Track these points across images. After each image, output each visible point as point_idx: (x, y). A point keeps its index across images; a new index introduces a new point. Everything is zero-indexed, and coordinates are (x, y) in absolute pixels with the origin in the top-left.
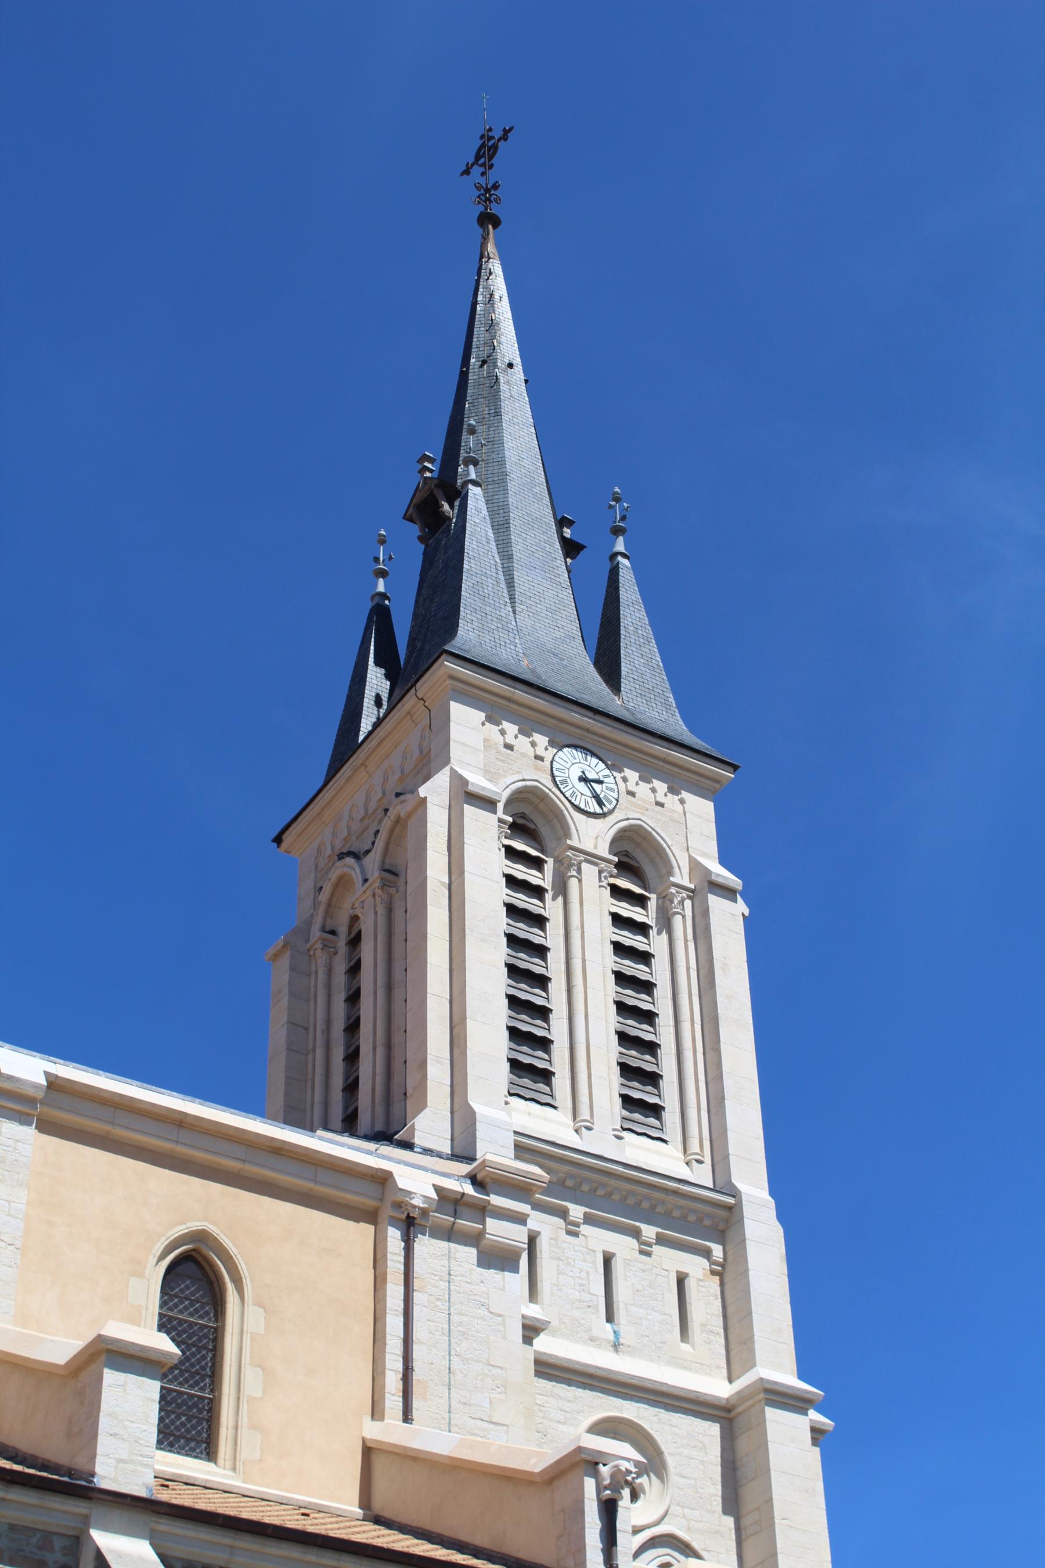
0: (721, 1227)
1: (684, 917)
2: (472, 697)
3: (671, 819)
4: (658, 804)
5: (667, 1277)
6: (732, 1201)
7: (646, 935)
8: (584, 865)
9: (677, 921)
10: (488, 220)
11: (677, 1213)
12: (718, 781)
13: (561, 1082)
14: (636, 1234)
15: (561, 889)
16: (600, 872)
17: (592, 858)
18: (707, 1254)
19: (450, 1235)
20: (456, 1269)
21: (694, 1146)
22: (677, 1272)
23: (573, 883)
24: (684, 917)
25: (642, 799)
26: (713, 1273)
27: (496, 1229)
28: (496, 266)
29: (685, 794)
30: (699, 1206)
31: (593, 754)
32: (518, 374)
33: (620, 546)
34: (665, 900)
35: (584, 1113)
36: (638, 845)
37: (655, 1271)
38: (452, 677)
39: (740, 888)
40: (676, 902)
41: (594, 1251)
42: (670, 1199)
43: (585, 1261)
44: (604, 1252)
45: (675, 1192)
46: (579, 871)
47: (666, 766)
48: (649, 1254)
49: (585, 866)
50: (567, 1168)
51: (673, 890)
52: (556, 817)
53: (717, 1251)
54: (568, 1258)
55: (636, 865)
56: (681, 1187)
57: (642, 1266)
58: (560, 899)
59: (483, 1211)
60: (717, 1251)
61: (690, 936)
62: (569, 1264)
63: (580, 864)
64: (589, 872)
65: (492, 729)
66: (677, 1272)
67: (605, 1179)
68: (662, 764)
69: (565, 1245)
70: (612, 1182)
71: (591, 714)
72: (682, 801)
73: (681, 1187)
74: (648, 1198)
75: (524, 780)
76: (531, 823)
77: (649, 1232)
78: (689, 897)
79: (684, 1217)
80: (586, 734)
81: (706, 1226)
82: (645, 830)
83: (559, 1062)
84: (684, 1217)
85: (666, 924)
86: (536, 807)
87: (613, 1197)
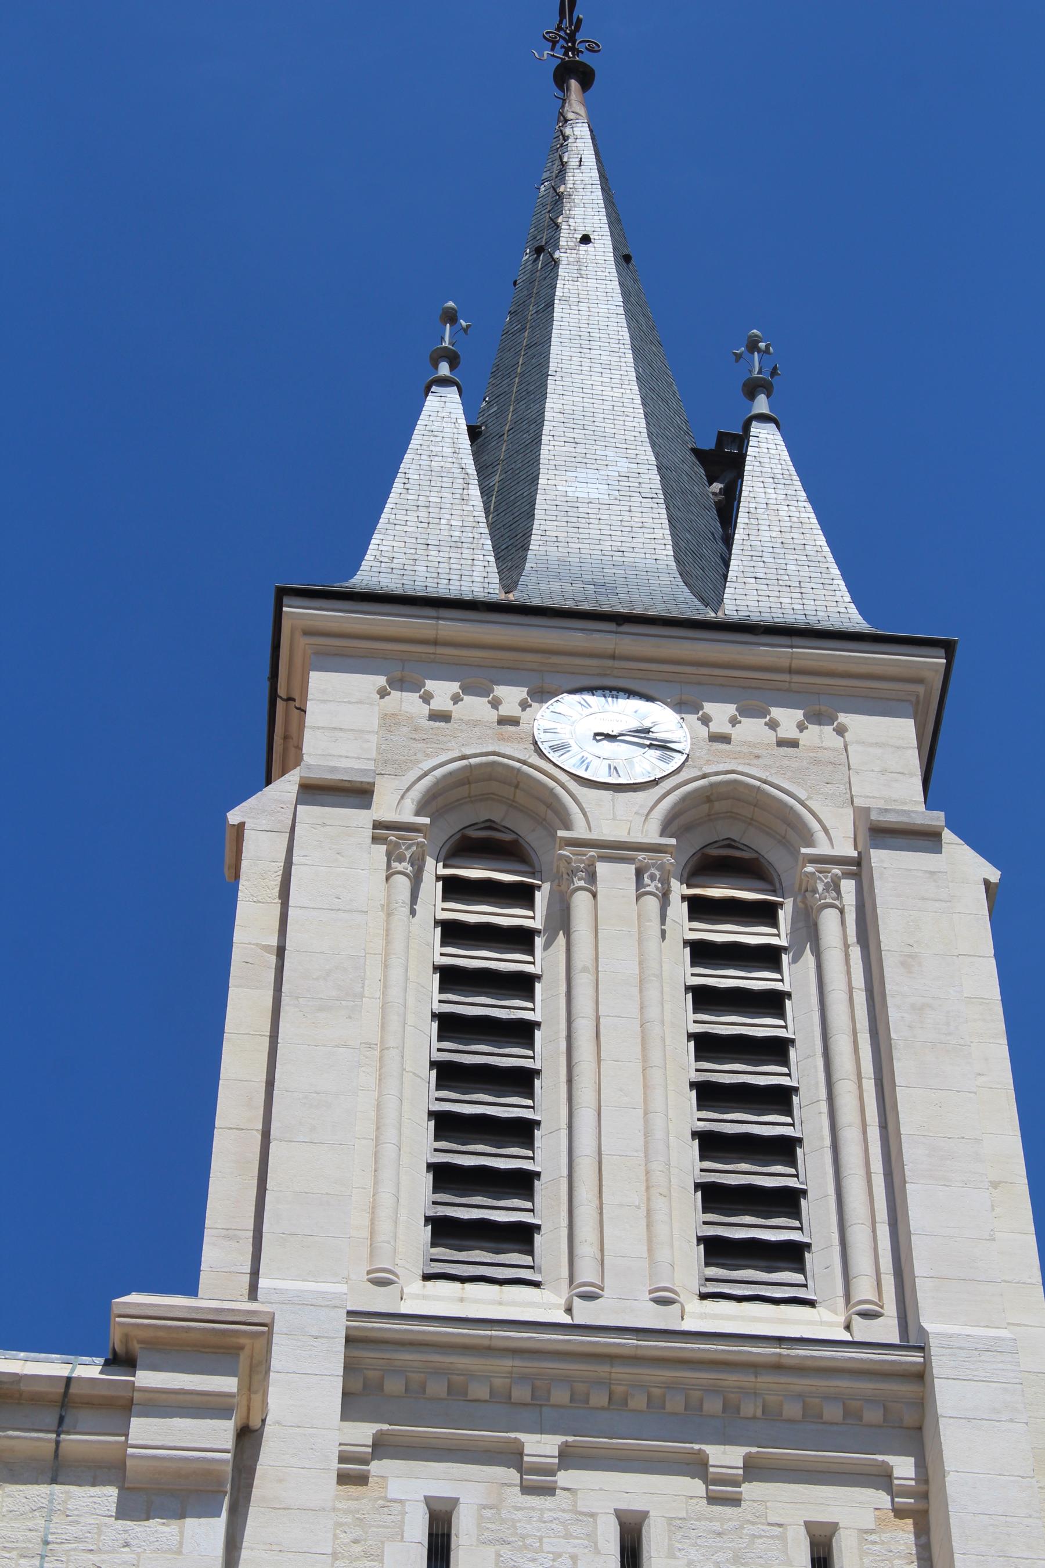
0: (909, 1419)
1: (842, 912)
2: (345, 655)
3: (816, 762)
4: (781, 743)
5: (783, 1538)
6: (917, 1358)
7: (777, 967)
8: (601, 868)
9: (829, 923)
10: (573, 72)
11: (793, 1410)
12: (920, 681)
13: (549, 1244)
14: (698, 1467)
15: (561, 920)
16: (639, 874)
17: (617, 851)
18: (883, 1479)
19: (57, 1470)
20: (59, 1527)
21: (864, 1290)
22: (808, 1524)
23: (581, 902)
24: (842, 912)
25: (744, 743)
26: (899, 1513)
27: (145, 1432)
28: (586, 208)
29: (843, 718)
30: (843, 1384)
31: (631, 693)
32: (603, 247)
33: (761, 404)
34: (805, 891)
35: (587, 1273)
36: (751, 822)
37: (749, 1529)
38: (308, 633)
39: (942, 823)
40: (820, 887)
41: (593, 1515)
42: (765, 1380)
43: (568, 1536)
44: (619, 1514)
45: (778, 1367)
46: (592, 877)
47: (796, 678)
48: (735, 1501)
49: (602, 869)
50: (507, 1364)
51: (810, 869)
52: (549, 806)
53: (903, 1467)
54: (523, 1537)
55: (753, 855)
56: (785, 1352)
57: (716, 1526)
58: (561, 939)
59: (122, 1407)
60: (903, 1467)
61: (852, 938)
62: (526, 1547)
63: (592, 865)
64: (615, 878)
65: (409, 703)
66: (808, 1524)
67: (602, 1370)
68: (786, 677)
69: (519, 1514)
70: (619, 1372)
71: (612, 626)
72: (841, 731)
73: (785, 1352)
74: (713, 1390)
75: (463, 757)
76: (492, 843)
77: (727, 1457)
78: (847, 875)
79: (731, 1408)
80: (610, 663)
81: (870, 1426)
82: (753, 787)
83: (546, 1209)
84: (811, 1415)
85: (808, 931)
86: (513, 805)
87: (632, 1404)
